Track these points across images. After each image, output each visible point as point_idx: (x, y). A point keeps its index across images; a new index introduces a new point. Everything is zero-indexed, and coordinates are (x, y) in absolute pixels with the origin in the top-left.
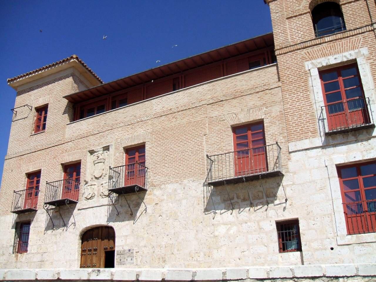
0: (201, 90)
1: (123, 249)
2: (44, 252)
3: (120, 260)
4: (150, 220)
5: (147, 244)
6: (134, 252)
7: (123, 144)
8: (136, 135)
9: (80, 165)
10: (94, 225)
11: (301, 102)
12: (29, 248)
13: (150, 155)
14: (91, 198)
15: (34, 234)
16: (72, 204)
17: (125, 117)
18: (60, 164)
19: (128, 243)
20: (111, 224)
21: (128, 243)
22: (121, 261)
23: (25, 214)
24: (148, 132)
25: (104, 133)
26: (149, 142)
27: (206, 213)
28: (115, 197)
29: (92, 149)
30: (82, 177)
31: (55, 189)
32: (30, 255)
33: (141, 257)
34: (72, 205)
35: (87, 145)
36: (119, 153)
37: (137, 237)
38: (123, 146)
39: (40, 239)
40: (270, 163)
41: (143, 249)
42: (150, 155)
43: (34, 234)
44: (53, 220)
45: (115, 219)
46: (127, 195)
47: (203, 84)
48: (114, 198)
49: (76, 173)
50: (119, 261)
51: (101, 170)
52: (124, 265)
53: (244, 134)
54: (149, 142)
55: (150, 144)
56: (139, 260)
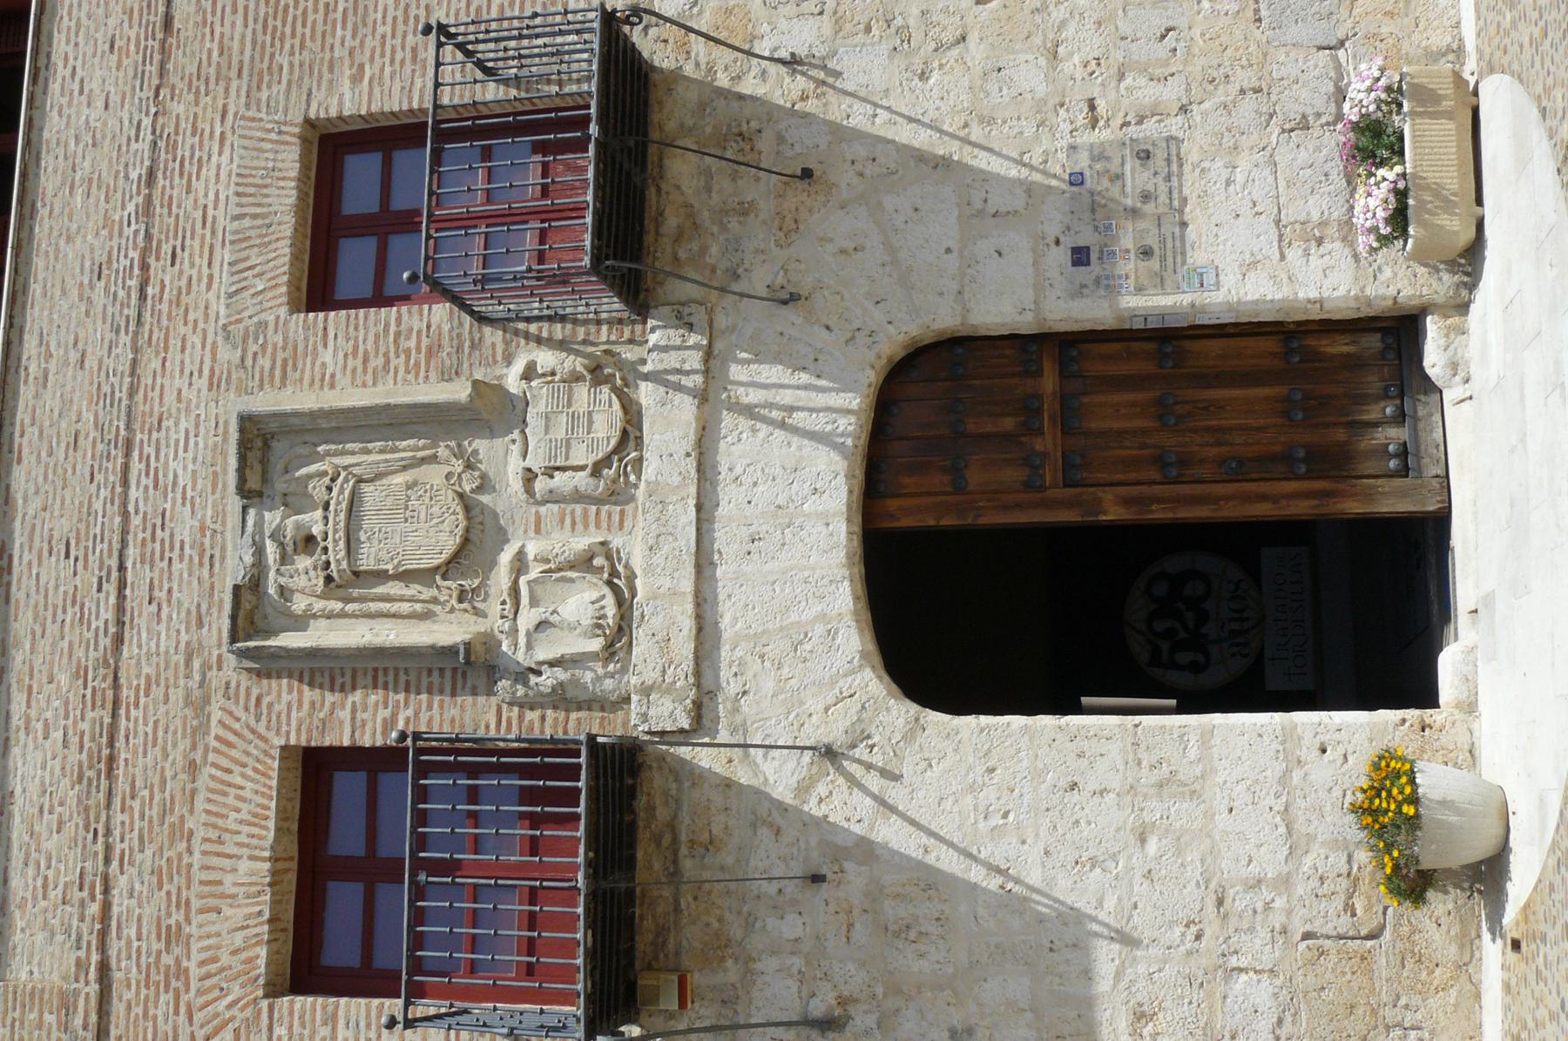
0: (149, 852)
4: (868, 29)
5: (1037, 40)
6: (1087, 138)
7: (263, 316)
8: (233, 188)
9: (330, 749)
11: (401, 27)
13: (408, 67)
14: (620, 583)
17: (74, 356)
18: (265, 1004)
24: (242, 110)
25: (136, 521)
26: (309, 95)
29: (228, 599)
30: (430, 708)
31: (450, 818)
33: (1128, 81)
34: (651, 808)
35: (177, 696)
36: (325, 346)
37: (981, 120)
38: (283, 312)
41: (1071, 65)
42: (408, 67)
44: (750, 1016)
45: (828, 328)
46: (657, 227)
51: (413, 503)
52: (1187, 218)
53: (511, 832)
54: (309, 95)
55: (331, 82)
56: (1148, 93)
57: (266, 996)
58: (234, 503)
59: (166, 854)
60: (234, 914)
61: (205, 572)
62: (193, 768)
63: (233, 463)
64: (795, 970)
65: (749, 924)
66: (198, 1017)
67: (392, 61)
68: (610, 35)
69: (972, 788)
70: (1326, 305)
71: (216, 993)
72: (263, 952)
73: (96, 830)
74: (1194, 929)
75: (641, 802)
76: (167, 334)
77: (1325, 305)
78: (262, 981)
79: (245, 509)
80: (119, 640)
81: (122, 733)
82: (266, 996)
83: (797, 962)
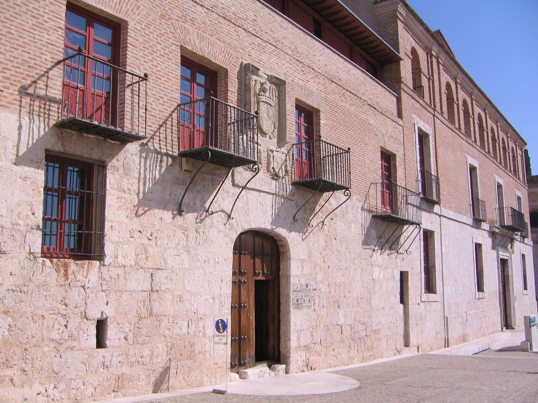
1: (299, 282)
2: (156, 267)
3: (297, 301)
10: (262, 228)
12: (481, 243)
15: (119, 208)
16: (217, 166)
19: (305, 273)
20: (282, 232)
21: (305, 273)
22: (298, 303)
23: (83, 136)
27: (364, 247)
28: (173, 152)
32: (114, 272)
39: (142, 230)
40: (192, 102)
43: (119, 208)
47: (358, 68)
48: (171, 149)
49: (87, 19)
50: (296, 302)
57: (181, 45)
58: (270, 74)
59: (208, 27)
60: (197, 42)
61: (257, 60)
62: (224, 42)
63: (418, 146)
64: (190, 203)
65: (199, 192)
66: (176, 22)
67: (342, 143)
68: (248, 162)
69: (222, 254)
70: (289, 342)
71: (181, 31)
72: (190, 48)
73: (212, 8)
74: (196, 312)
75: (220, 167)
76: (291, 64)
77: (289, 342)
78: (184, 46)
79: (267, 75)
80: (245, 30)
81: (208, 13)
82: (181, 45)
83: (191, 204)
